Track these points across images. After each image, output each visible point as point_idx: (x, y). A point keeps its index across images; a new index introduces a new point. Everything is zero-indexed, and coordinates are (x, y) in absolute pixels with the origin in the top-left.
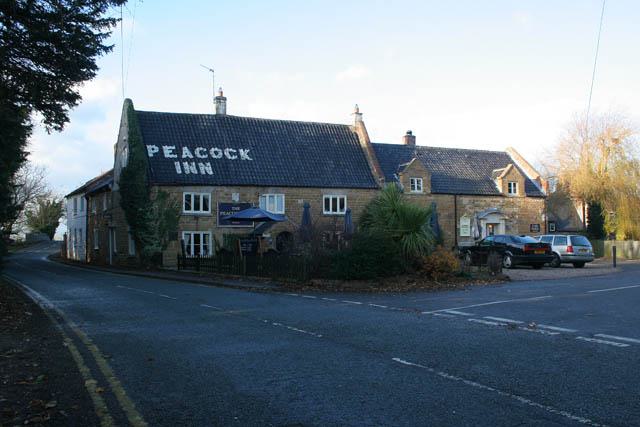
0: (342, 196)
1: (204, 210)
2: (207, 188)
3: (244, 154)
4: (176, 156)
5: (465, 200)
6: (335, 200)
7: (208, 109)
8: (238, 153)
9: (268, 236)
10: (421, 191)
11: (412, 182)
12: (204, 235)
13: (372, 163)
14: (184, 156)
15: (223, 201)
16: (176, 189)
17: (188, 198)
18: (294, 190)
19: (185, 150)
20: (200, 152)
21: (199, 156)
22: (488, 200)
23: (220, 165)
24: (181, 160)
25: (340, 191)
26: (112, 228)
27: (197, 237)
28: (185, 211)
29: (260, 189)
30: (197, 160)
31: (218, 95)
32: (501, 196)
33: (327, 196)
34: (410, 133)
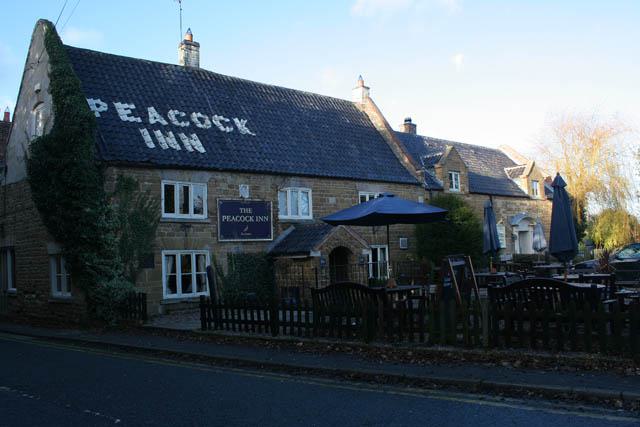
2: (200, 173)
3: (241, 124)
4: (139, 120)
5: (499, 202)
7: (175, 57)
8: (232, 123)
9: (318, 254)
12: (197, 257)
13: (398, 150)
16: (149, 174)
18: (324, 184)
19: (152, 112)
20: (177, 116)
22: (518, 202)
23: (208, 136)
24: (145, 124)
27: (186, 260)
28: (165, 215)
29: (279, 179)
31: (187, 38)
32: (528, 198)
34: (410, 120)
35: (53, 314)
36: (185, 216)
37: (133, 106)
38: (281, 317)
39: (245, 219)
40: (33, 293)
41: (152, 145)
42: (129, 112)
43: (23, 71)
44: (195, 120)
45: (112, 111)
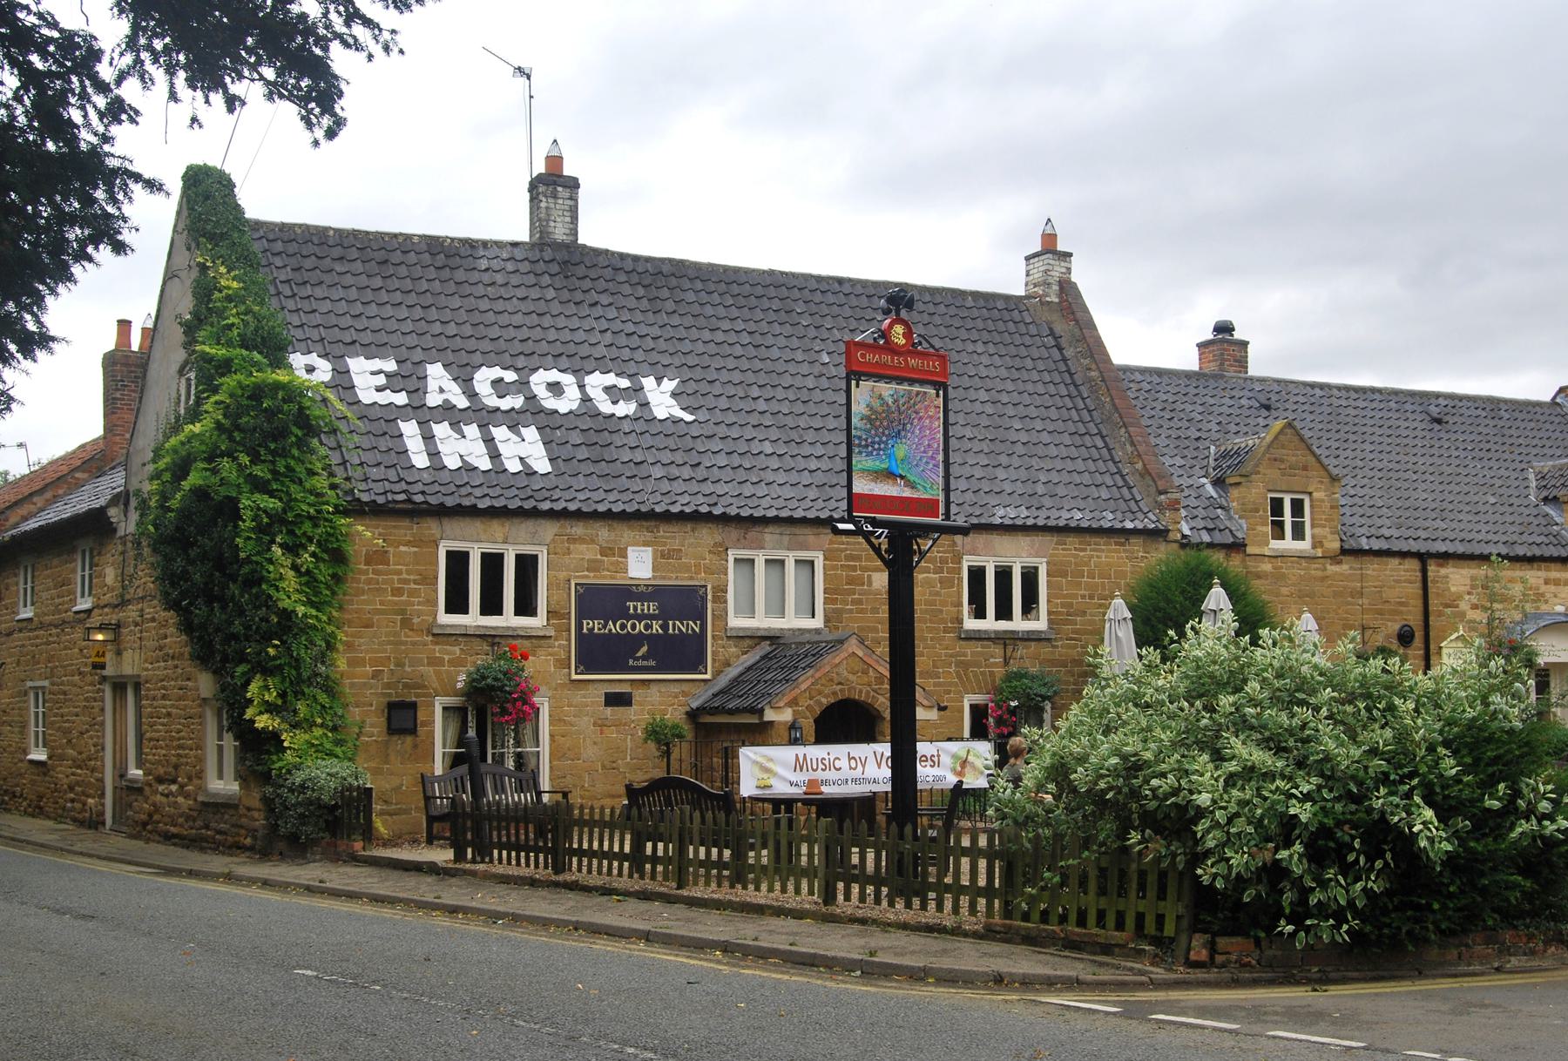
0: (1031, 561)
1: (518, 612)
3: (662, 399)
4: (401, 399)
5: (1456, 579)
6: (1004, 576)
10: (1304, 546)
11: (1277, 507)
14: (433, 400)
15: (592, 579)
17: (458, 562)
19: (436, 374)
20: (497, 383)
21: (492, 401)
24: (419, 411)
25: (1024, 541)
26: (119, 687)
28: (445, 619)
30: (485, 417)
33: (976, 561)
35: (207, 827)
36: (492, 621)
37: (391, 366)
38: (855, 860)
39: (640, 627)
40: (174, 781)
41: (420, 460)
42: (382, 380)
43: (160, 283)
44: (541, 391)
45: (343, 382)
